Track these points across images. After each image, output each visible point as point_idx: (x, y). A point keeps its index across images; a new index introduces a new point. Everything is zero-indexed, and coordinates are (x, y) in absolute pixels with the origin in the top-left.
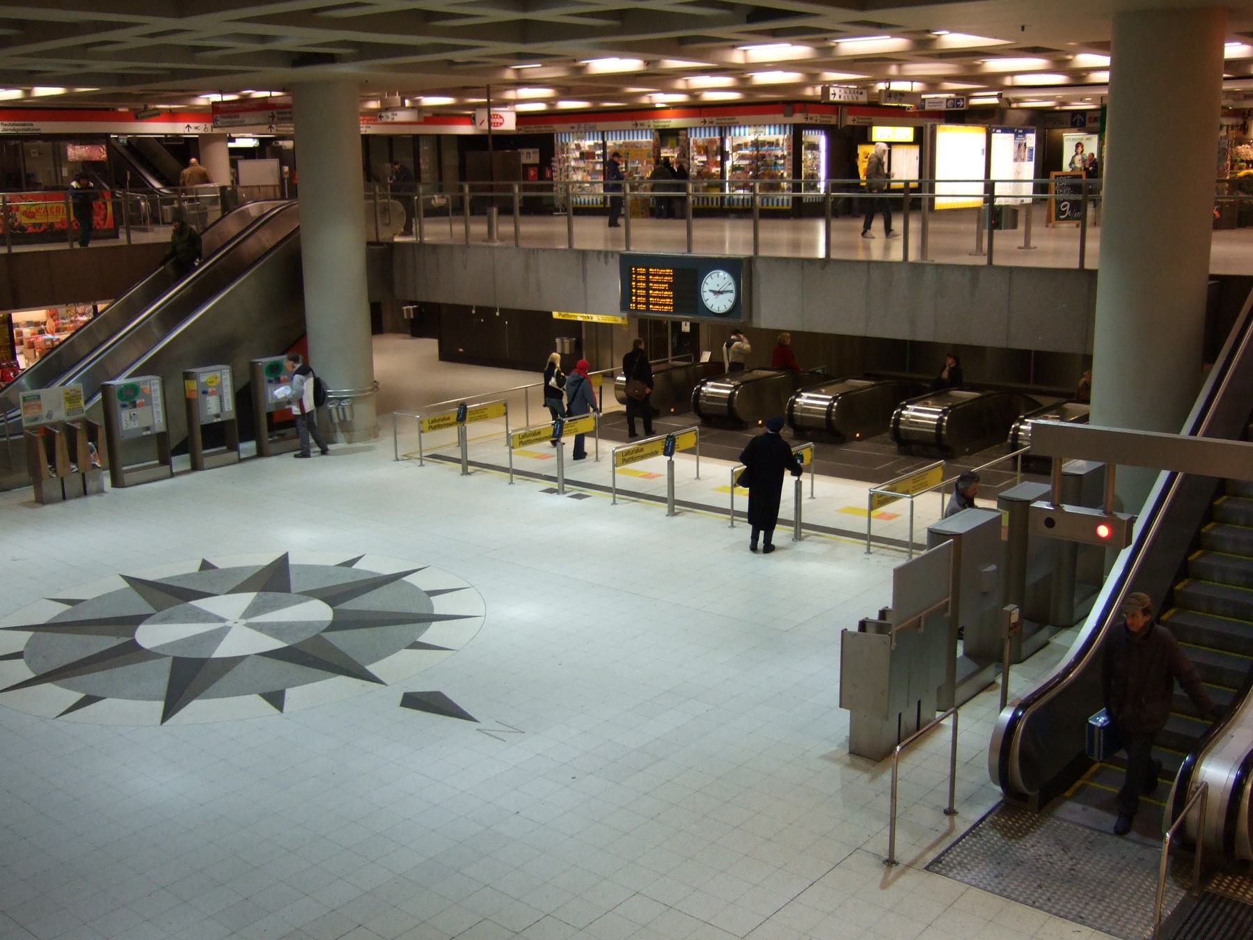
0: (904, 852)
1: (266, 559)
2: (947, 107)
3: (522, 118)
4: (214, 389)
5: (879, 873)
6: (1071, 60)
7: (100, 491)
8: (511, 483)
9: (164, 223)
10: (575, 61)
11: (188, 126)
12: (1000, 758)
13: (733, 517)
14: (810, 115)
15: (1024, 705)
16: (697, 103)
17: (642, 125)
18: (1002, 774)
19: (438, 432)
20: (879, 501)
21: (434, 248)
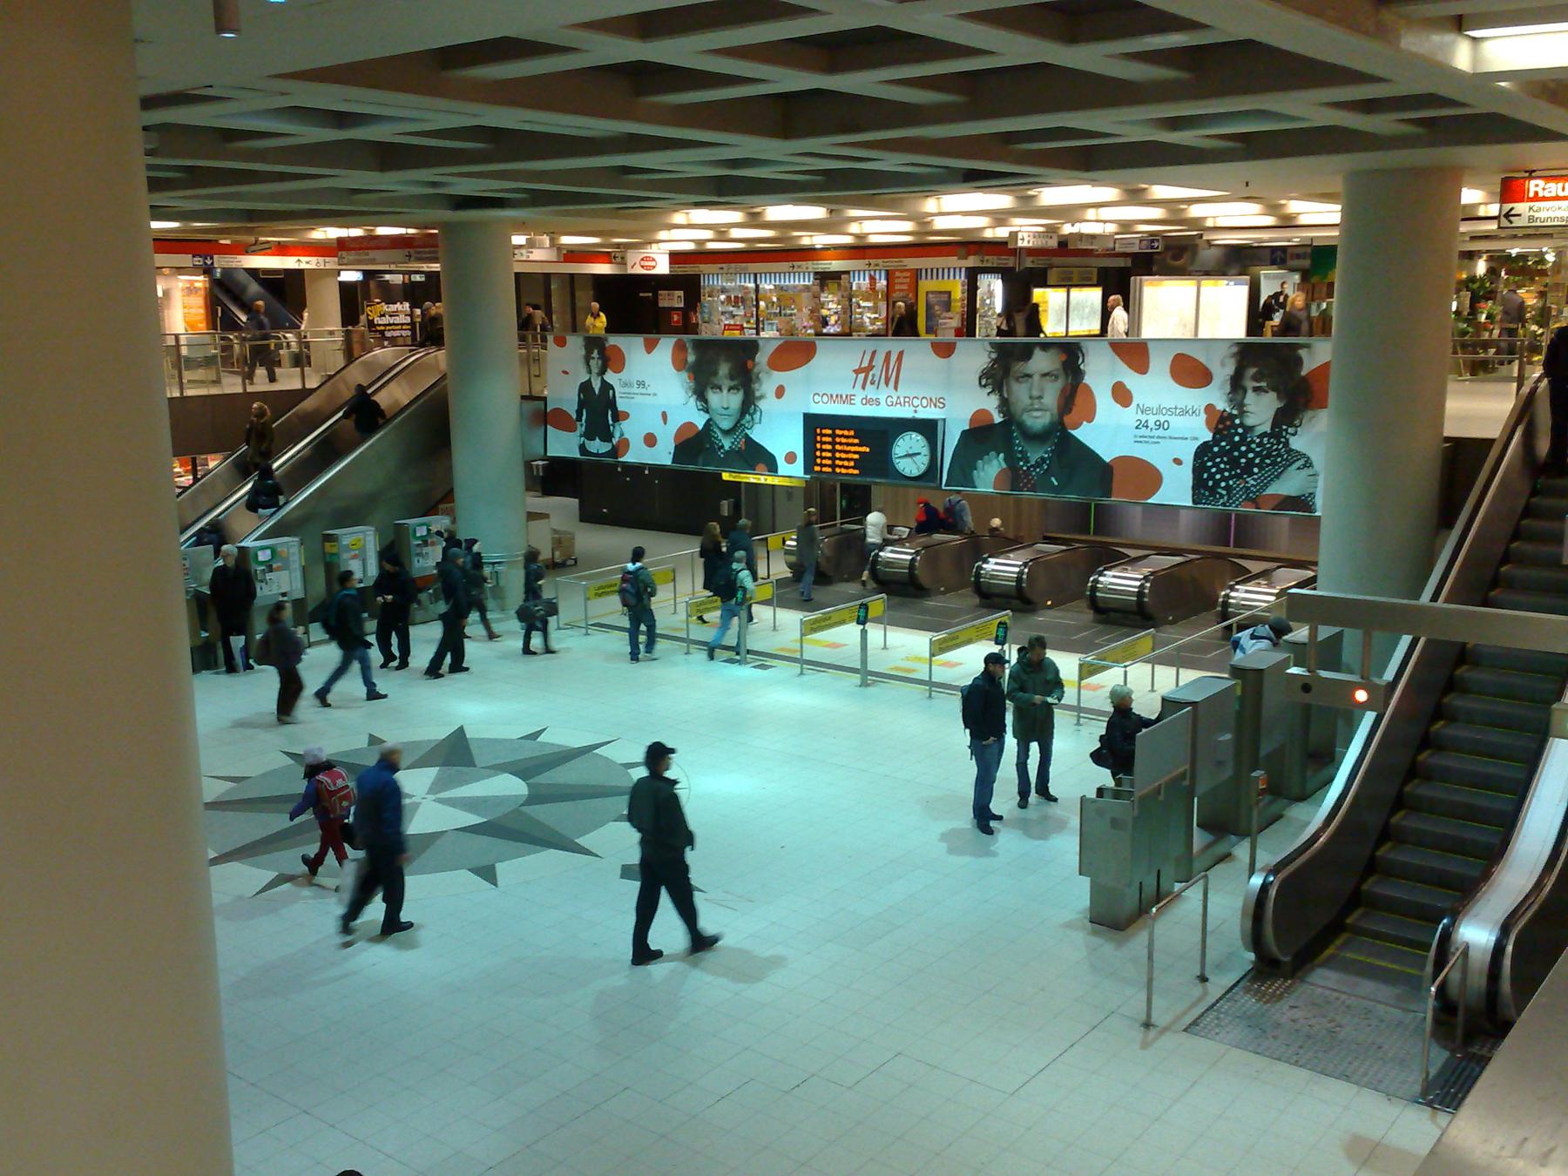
0: (1159, 1018)
1: (442, 733)
2: (1140, 249)
3: (675, 257)
4: (357, 552)
5: (1138, 1034)
6: (1284, 205)
8: (688, 653)
11: (299, 260)
12: (1253, 924)
13: (930, 689)
14: (987, 258)
15: (1275, 870)
16: (862, 245)
17: (799, 267)
18: (1256, 940)
19: (601, 600)
20: (1089, 671)
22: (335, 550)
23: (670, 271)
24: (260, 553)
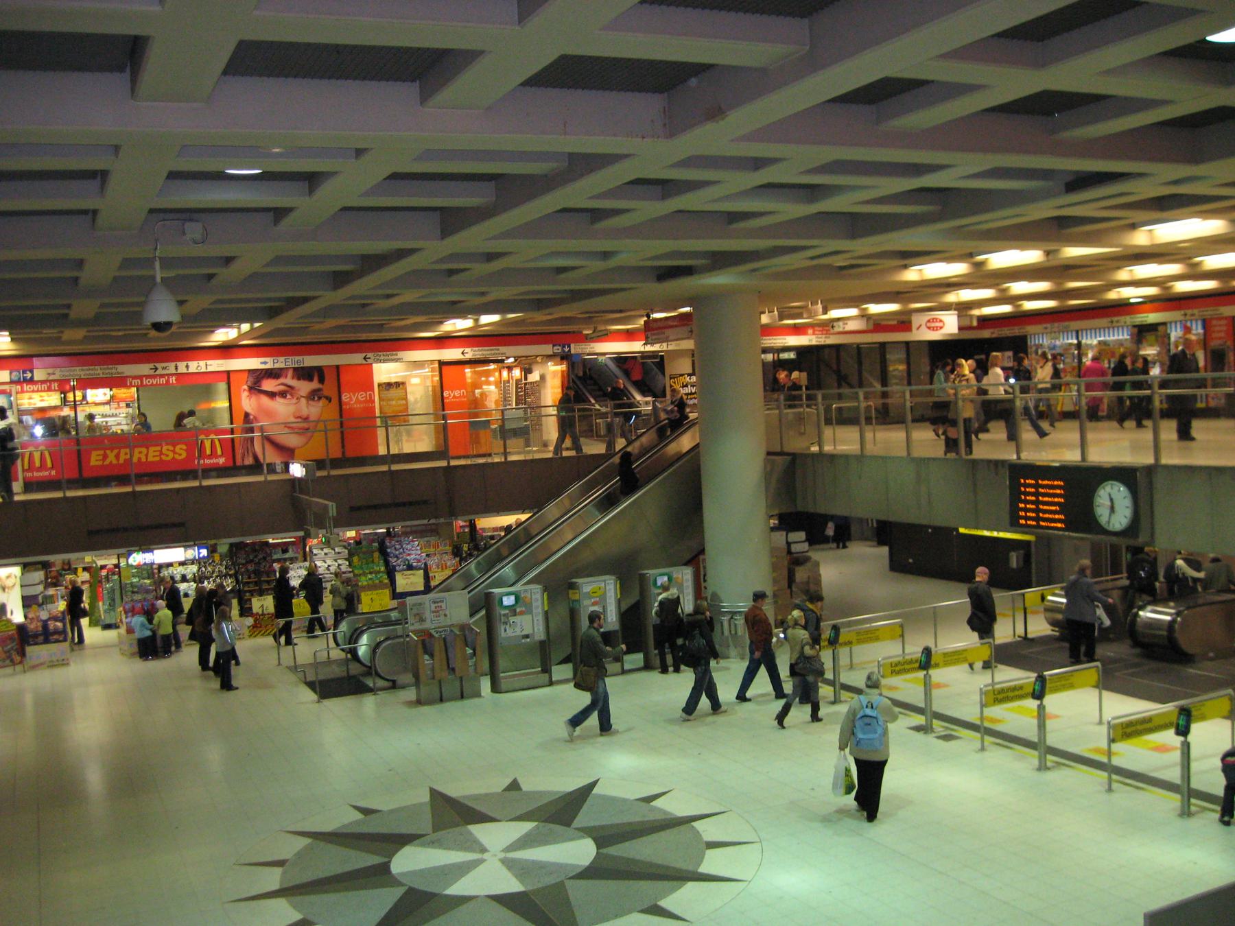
7: (478, 694)
9: (598, 436)
10: (1190, 258)
21: (832, 457)
22: (577, 597)
23: (960, 328)
24: (505, 599)
